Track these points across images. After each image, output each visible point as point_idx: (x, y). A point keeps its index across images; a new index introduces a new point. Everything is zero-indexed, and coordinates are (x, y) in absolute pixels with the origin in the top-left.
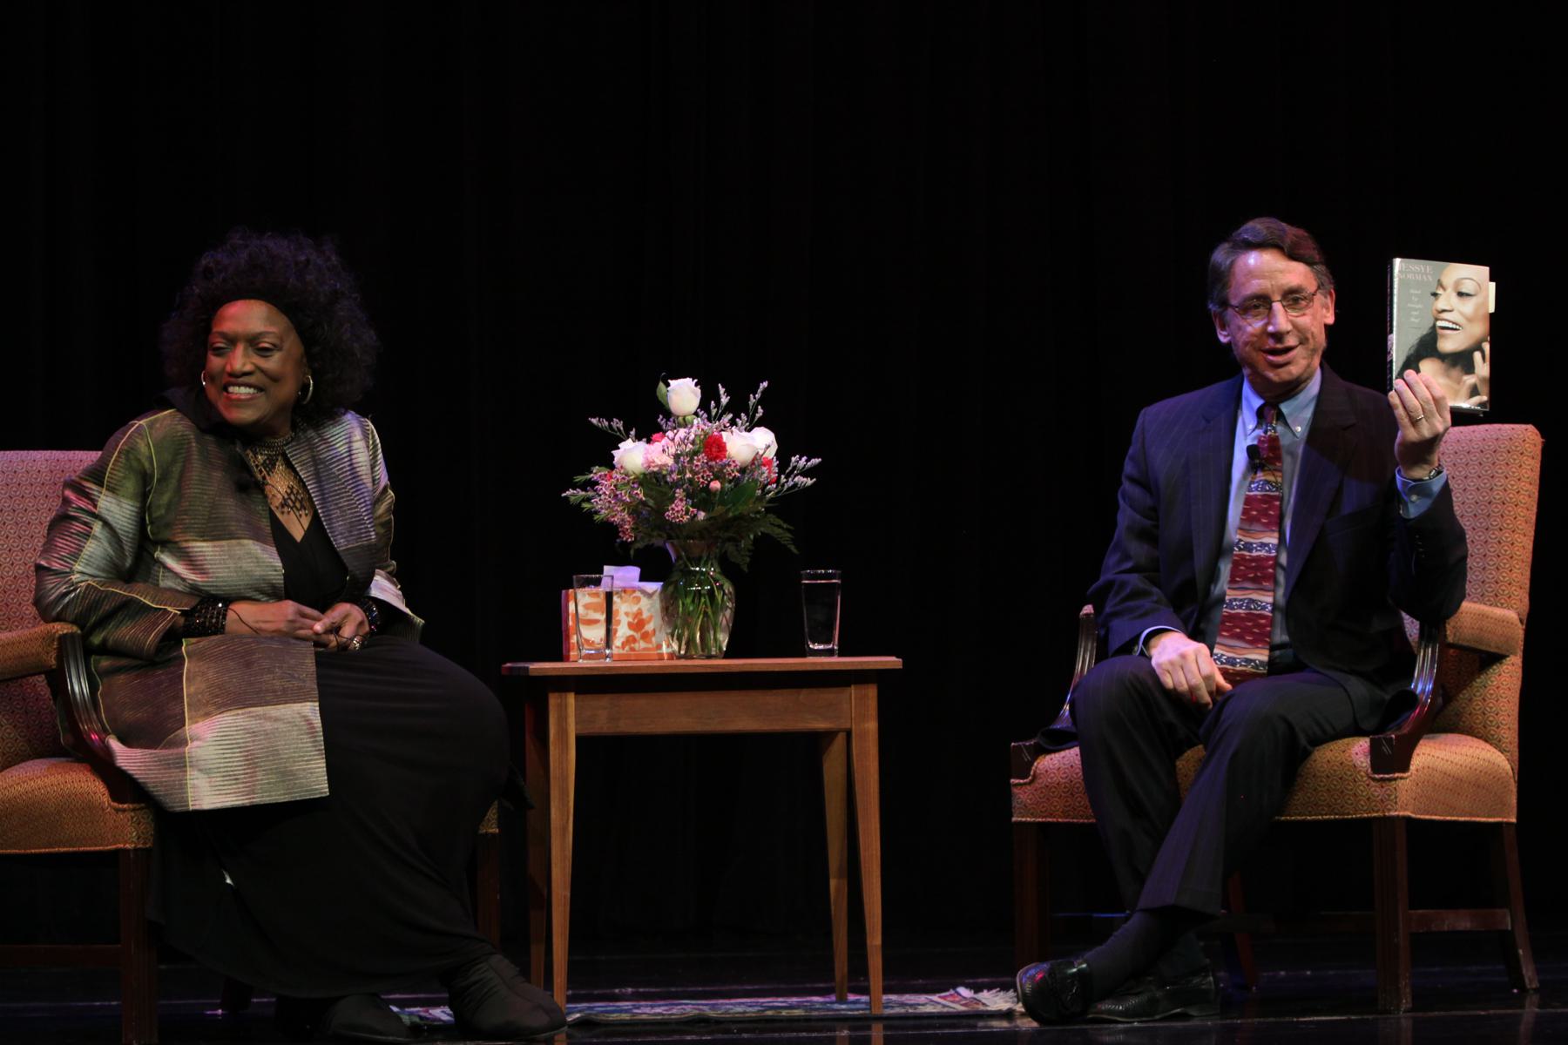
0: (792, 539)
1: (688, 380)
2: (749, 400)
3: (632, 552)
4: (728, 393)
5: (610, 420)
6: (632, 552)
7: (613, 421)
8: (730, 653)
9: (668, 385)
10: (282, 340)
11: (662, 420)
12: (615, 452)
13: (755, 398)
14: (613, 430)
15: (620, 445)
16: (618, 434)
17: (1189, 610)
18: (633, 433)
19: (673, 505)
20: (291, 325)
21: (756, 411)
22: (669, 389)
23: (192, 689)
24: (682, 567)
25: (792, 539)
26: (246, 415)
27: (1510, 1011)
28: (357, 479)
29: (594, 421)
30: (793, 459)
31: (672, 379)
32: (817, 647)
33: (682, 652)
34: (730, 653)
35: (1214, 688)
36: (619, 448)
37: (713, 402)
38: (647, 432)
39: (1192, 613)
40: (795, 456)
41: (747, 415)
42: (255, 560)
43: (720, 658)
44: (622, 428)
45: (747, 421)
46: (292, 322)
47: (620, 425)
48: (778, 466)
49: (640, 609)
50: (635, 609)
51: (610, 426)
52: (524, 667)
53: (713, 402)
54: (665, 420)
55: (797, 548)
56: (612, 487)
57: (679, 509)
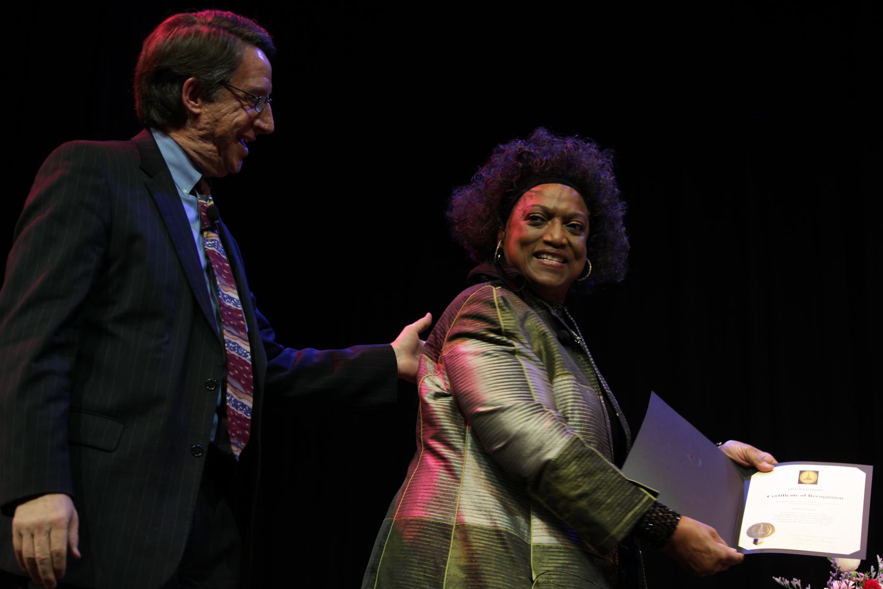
5: (790, 580)
7: (792, 580)
8: (242, 314)
17: (206, 78)
27: (600, 454)
28: (454, 371)
29: (778, 580)
32: (223, 276)
34: (242, 314)
35: (544, 442)
37: (872, 567)
39: (206, 77)
42: (443, 331)
51: (791, 584)
53: (872, 567)
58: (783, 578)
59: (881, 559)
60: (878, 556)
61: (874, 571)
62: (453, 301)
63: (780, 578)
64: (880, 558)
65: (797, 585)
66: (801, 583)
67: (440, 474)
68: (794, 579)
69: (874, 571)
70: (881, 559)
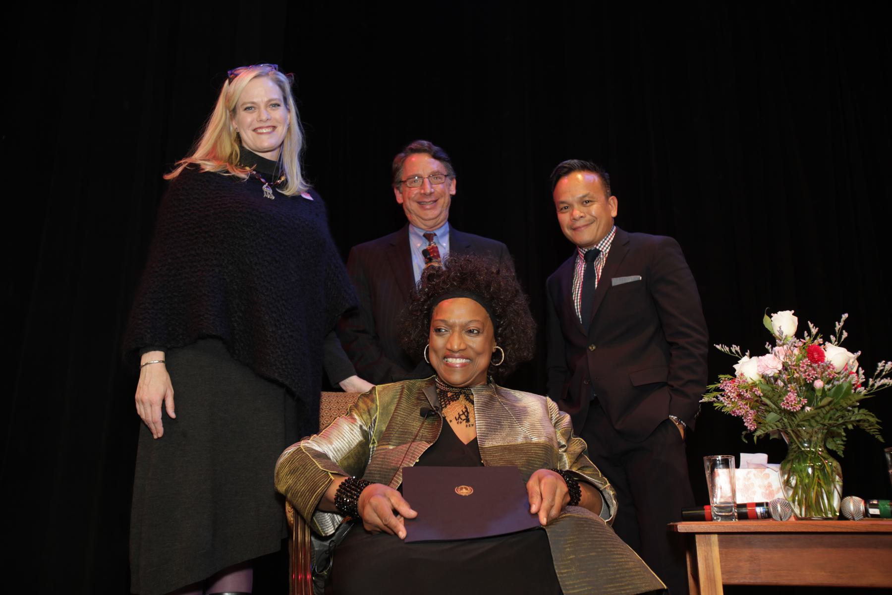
0: (880, 430)
1: (788, 312)
2: (835, 326)
3: (755, 438)
4: (815, 326)
5: (730, 346)
6: (755, 438)
9: (771, 317)
10: (484, 326)
11: (769, 346)
12: (735, 366)
13: (839, 325)
14: (733, 353)
15: (739, 362)
16: (737, 355)
18: (748, 354)
19: (787, 397)
20: (488, 315)
21: (841, 334)
22: (772, 319)
23: (814, 516)
24: (796, 449)
25: (880, 430)
26: (457, 378)
29: (719, 347)
30: (880, 364)
31: (774, 313)
33: (803, 515)
36: (738, 363)
37: (806, 332)
38: (759, 351)
40: (880, 362)
41: (835, 336)
43: (836, 520)
44: (739, 351)
45: (836, 341)
46: (488, 312)
47: (738, 349)
48: (864, 374)
49: (769, 483)
50: (766, 483)
51: (730, 350)
52: (673, 525)
53: (806, 332)
54: (770, 346)
55: (883, 437)
56: (736, 388)
57: (792, 400)
58: (723, 345)
59: (813, 325)
60: (809, 322)
61: (808, 336)
62: (364, 243)
63: (720, 345)
64: (811, 323)
65: (736, 351)
66: (740, 349)
67: (403, 413)
68: (733, 346)
69: (808, 336)
70: (813, 325)
